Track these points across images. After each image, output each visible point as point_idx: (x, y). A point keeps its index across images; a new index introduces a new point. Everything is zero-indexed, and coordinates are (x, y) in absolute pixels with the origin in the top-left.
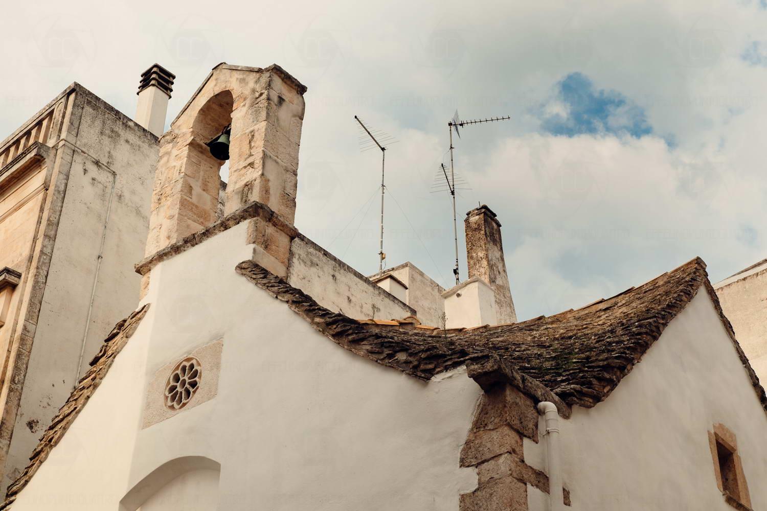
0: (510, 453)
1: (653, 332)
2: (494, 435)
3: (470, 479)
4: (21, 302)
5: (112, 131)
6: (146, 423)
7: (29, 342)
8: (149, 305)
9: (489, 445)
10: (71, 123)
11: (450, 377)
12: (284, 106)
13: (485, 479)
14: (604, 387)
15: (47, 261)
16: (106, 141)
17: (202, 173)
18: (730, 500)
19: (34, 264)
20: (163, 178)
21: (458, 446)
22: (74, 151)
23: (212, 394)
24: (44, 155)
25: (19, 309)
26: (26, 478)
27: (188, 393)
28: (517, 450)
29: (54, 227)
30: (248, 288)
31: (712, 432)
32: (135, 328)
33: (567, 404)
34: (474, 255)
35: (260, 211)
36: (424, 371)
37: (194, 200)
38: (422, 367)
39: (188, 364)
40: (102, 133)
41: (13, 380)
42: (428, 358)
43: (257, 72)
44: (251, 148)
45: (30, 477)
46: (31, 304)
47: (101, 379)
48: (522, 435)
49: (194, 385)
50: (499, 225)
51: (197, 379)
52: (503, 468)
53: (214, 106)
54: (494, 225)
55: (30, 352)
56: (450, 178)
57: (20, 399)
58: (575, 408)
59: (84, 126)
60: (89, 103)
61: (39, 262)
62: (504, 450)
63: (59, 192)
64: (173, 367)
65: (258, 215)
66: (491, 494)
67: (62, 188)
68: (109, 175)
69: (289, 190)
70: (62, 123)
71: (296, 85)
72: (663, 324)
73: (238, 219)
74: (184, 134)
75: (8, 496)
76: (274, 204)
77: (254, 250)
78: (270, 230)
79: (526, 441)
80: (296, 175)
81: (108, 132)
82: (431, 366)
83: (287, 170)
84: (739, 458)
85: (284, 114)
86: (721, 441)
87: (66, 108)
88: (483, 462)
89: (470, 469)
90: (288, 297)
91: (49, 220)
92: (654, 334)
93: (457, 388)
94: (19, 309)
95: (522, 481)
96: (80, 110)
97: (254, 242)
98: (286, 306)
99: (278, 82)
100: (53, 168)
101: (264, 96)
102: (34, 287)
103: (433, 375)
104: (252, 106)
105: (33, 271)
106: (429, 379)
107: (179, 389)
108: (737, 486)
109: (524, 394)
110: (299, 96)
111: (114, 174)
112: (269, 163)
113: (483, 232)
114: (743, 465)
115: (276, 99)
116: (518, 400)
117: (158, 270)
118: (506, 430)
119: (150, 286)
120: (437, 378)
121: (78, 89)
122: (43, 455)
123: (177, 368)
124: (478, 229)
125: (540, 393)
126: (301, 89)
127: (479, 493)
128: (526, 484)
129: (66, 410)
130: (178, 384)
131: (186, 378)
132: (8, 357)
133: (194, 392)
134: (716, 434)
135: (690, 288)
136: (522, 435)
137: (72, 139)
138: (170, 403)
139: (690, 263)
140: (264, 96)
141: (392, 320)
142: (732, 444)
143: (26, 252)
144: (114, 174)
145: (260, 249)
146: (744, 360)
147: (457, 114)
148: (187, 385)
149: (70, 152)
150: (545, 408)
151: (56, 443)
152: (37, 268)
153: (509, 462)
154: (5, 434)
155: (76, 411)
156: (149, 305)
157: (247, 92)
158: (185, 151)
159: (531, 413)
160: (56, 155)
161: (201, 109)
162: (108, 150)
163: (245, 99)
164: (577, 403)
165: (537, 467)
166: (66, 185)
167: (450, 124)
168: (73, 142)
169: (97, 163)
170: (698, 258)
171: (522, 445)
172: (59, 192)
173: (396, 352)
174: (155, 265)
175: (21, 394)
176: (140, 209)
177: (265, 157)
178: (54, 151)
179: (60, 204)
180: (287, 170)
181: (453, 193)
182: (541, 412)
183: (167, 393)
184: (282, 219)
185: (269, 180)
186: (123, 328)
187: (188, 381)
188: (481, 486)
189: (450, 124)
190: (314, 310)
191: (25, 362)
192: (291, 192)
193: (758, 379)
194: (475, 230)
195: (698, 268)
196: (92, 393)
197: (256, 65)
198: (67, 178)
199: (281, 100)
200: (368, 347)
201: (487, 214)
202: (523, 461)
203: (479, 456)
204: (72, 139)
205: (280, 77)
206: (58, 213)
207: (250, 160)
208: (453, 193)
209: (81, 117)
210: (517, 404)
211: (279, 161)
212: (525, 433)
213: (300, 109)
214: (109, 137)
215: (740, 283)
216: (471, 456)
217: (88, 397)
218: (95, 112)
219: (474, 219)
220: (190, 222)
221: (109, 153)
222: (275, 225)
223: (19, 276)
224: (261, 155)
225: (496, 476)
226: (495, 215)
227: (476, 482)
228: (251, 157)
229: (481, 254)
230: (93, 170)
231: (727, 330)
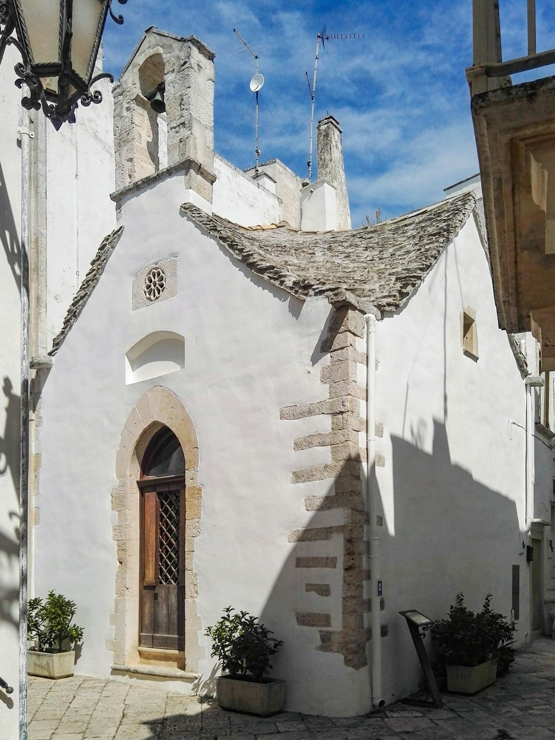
23: (173, 294)
29: (44, 154)
53: (150, 65)
93: (293, 708)
107: (152, 287)
129: (82, 293)
133: (163, 291)
141: (272, 224)
154: (42, 305)
176: (97, 133)
179: (44, 135)
183: (146, 290)
187: (157, 282)
207: (182, 120)
211: (201, 120)
220: (143, 163)
228: (182, 118)
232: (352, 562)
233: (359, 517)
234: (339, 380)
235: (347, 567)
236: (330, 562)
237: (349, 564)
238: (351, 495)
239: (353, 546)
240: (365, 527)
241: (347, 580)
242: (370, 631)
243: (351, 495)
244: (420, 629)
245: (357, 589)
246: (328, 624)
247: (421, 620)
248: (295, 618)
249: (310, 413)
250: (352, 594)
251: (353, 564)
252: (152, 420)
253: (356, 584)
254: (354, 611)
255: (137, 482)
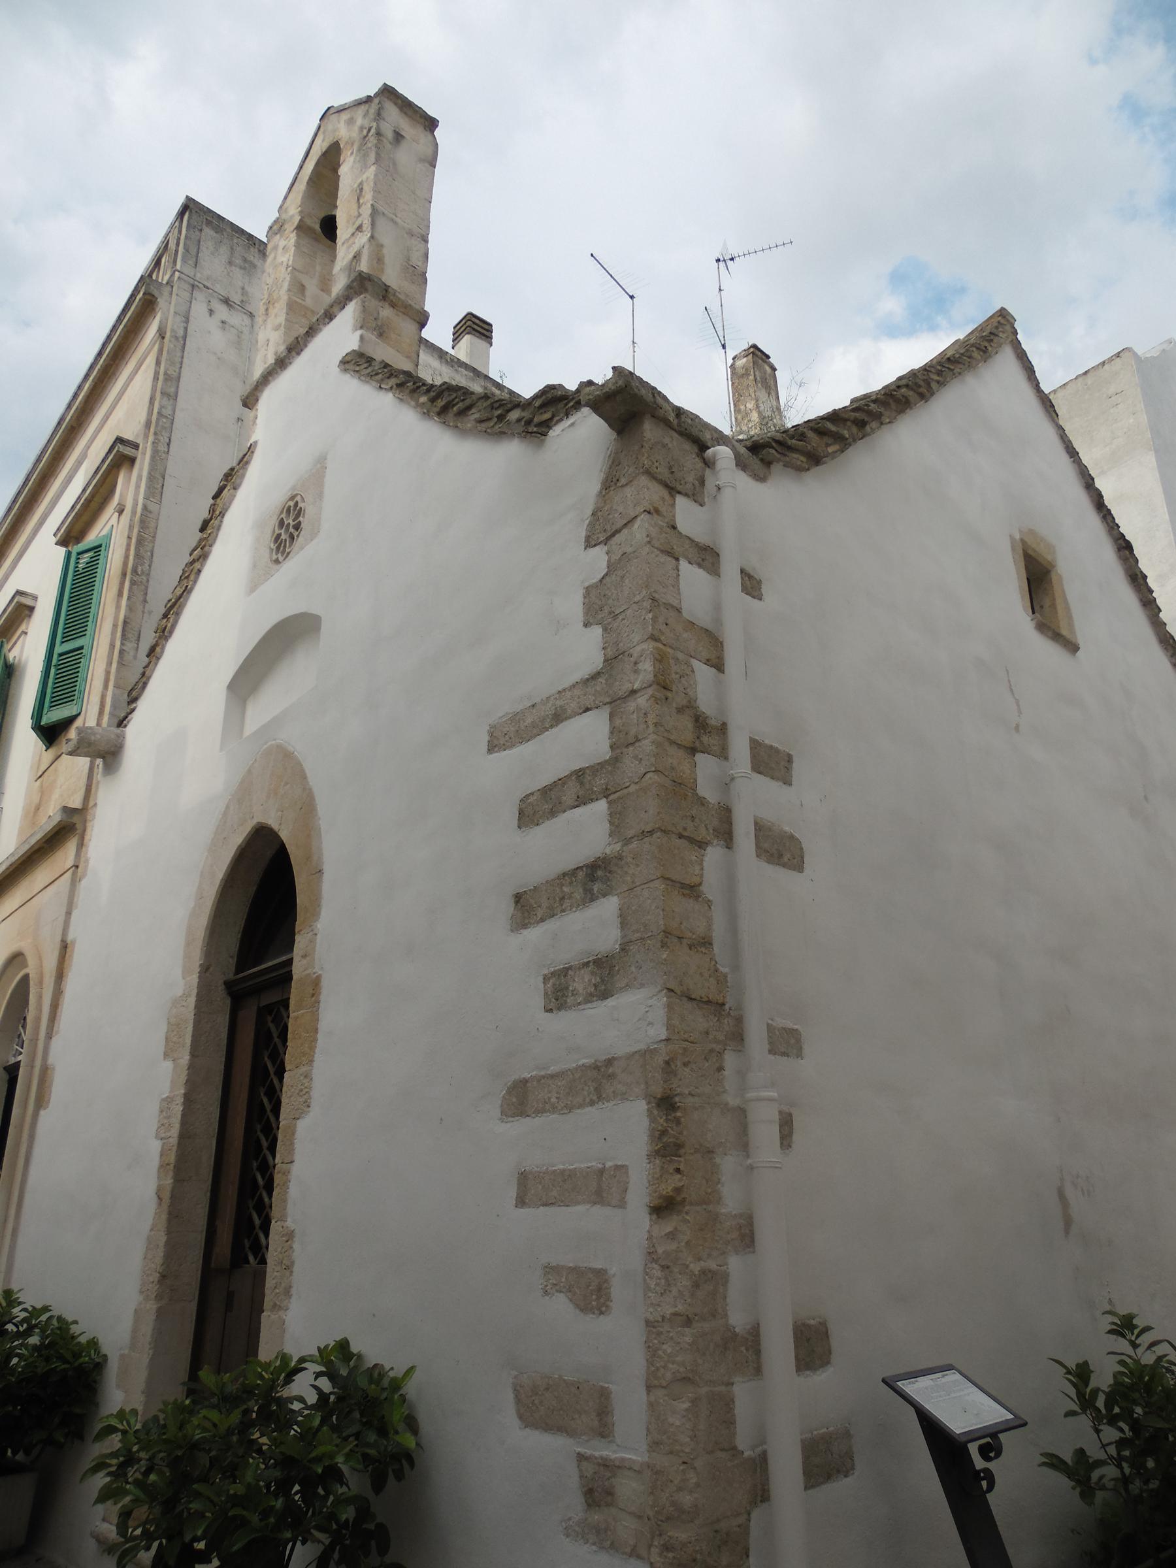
0: (649, 513)
1: (920, 386)
2: (629, 492)
3: (598, 559)
4: (140, 477)
5: (245, 260)
6: (253, 587)
7: (152, 525)
8: (256, 443)
9: (621, 509)
10: (187, 250)
11: (572, 424)
12: (404, 145)
13: (615, 557)
14: (828, 445)
15: (168, 425)
16: (237, 273)
17: (318, 268)
18: (1042, 627)
19: (152, 430)
20: (270, 281)
21: (583, 521)
22: (193, 286)
23: (314, 535)
24: (155, 292)
25: (138, 487)
26: (144, 679)
27: (292, 537)
28: (663, 509)
30: (355, 388)
31: (1018, 537)
32: (243, 476)
33: (762, 460)
34: (742, 407)
35: (368, 285)
36: (540, 424)
37: (309, 302)
38: (536, 420)
39: (291, 504)
40: (230, 263)
41: (135, 571)
42: (541, 407)
43: (366, 102)
44: (359, 207)
45: (149, 678)
46: (151, 478)
47: (211, 546)
48: (673, 491)
49: (297, 527)
50: (774, 369)
51: (301, 519)
52: (638, 536)
54: (767, 368)
55: (154, 537)
56: (719, 326)
57: (146, 594)
58: (777, 468)
59: (205, 255)
60: (209, 223)
61: (156, 426)
62: (640, 509)
63: (177, 338)
64: (278, 511)
65: (366, 290)
66: (622, 577)
67: (181, 333)
68: (245, 317)
69: (416, 260)
70: (177, 251)
71: (421, 117)
72: (938, 382)
73: (342, 302)
74: (293, 216)
75: (129, 703)
76: (392, 277)
77: (362, 337)
78: (386, 312)
79: (680, 500)
80: (426, 241)
81: (238, 261)
82: (547, 416)
83: (411, 234)
84: (1060, 577)
85: (405, 156)
86: (1030, 552)
87: (180, 232)
88: (613, 535)
89: (597, 548)
90: (393, 382)
91: (165, 374)
92: (921, 390)
94: (138, 487)
95: (669, 553)
96: (198, 233)
97: (361, 328)
98: (390, 395)
99: (392, 113)
100: (169, 310)
101: (373, 131)
102: (153, 458)
103: (550, 428)
104: (359, 150)
105: (151, 438)
106: (544, 434)
107: (283, 537)
108: (1056, 613)
109: (681, 434)
110: (428, 133)
111: (251, 315)
112: (381, 223)
113: (751, 377)
114: (1066, 587)
115: (389, 135)
116: (667, 440)
117: (267, 398)
118: (643, 480)
119: (258, 421)
120: (555, 431)
121: (191, 206)
122: (158, 649)
123: (282, 512)
124: (747, 374)
125: (708, 437)
126: (431, 124)
127: (608, 579)
128: (677, 559)
129: (179, 591)
130: (283, 531)
131: (290, 521)
132: (128, 545)
134: (1022, 540)
135: (986, 344)
136: (673, 491)
137: (189, 270)
138: (274, 557)
139: (991, 317)
140: (373, 131)
142: (1049, 558)
143: (143, 417)
144: (251, 315)
145: (371, 337)
146: (1072, 453)
147: (725, 244)
148: (291, 530)
149: (187, 287)
150: (714, 455)
151: (171, 632)
152: (155, 434)
153: (647, 525)
155: (187, 591)
156: (256, 443)
157: (355, 134)
158: (293, 237)
159: (690, 460)
160: (171, 294)
161: (310, 179)
162: (240, 284)
163: (353, 144)
164: (778, 461)
165: (702, 538)
166: (186, 329)
167: (718, 260)
168: (192, 275)
169: (226, 301)
170: (1003, 309)
171: (673, 505)
172: (177, 338)
173: (509, 411)
174: (262, 391)
175: (147, 588)
177: (375, 212)
178: (169, 288)
179: (179, 354)
180: (411, 234)
181: (724, 346)
182: (709, 464)
184: (402, 297)
185: (382, 246)
186: (231, 478)
188: (611, 568)
189: (718, 260)
190: (419, 387)
191: (148, 549)
192: (420, 264)
193: (1093, 479)
194: (743, 376)
195: (1002, 321)
196: (203, 565)
197: (362, 94)
198: (187, 320)
199: (398, 137)
200: (477, 416)
201: (757, 354)
202: (674, 527)
203: (608, 527)
204: (189, 270)
205: (396, 104)
206: (178, 365)
208: (724, 346)
209: (199, 241)
210: (664, 446)
211: (399, 220)
212: (679, 488)
213: (430, 151)
214: (241, 268)
215: (1080, 379)
216: (601, 530)
217: (199, 571)
218: (218, 236)
219: (741, 363)
221: (243, 289)
222: (393, 305)
223: (136, 446)
224: (369, 211)
225: (630, 550)
226: (768, 357)
227: (605, 564)
229: (750, 405)
230: (222, 311)
231: (1047, 411)
232: (675, 1181)
233: (699, 1021)
234: (624, 607)
235: (656, 1202)
236: (601, 1186)
237: (667, 1188)
238: (664, 945)
239: (678, 1121)
240: (730, 1059)
241: (660, 1251)
242: (760, 1464)
243: (664, 945)
244: (973, 1448)
245: (696, 1285)
246: (604, 1431)
247: (964, 1408)
248: (510, 1396)
249: (558, 718)
250: (680, 1308)
251: (678, 1190)
252: (255, 822)
253: (696, 1268)
254: (686, 1380)
255: (226, 983)
